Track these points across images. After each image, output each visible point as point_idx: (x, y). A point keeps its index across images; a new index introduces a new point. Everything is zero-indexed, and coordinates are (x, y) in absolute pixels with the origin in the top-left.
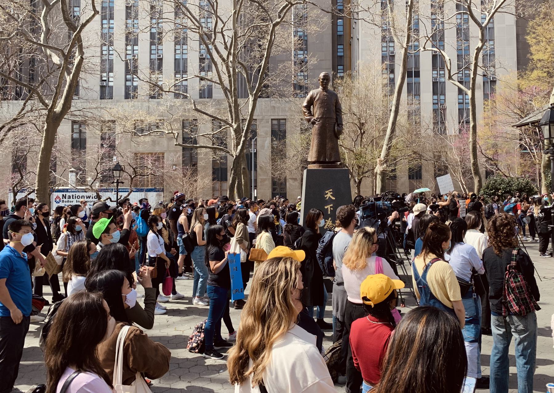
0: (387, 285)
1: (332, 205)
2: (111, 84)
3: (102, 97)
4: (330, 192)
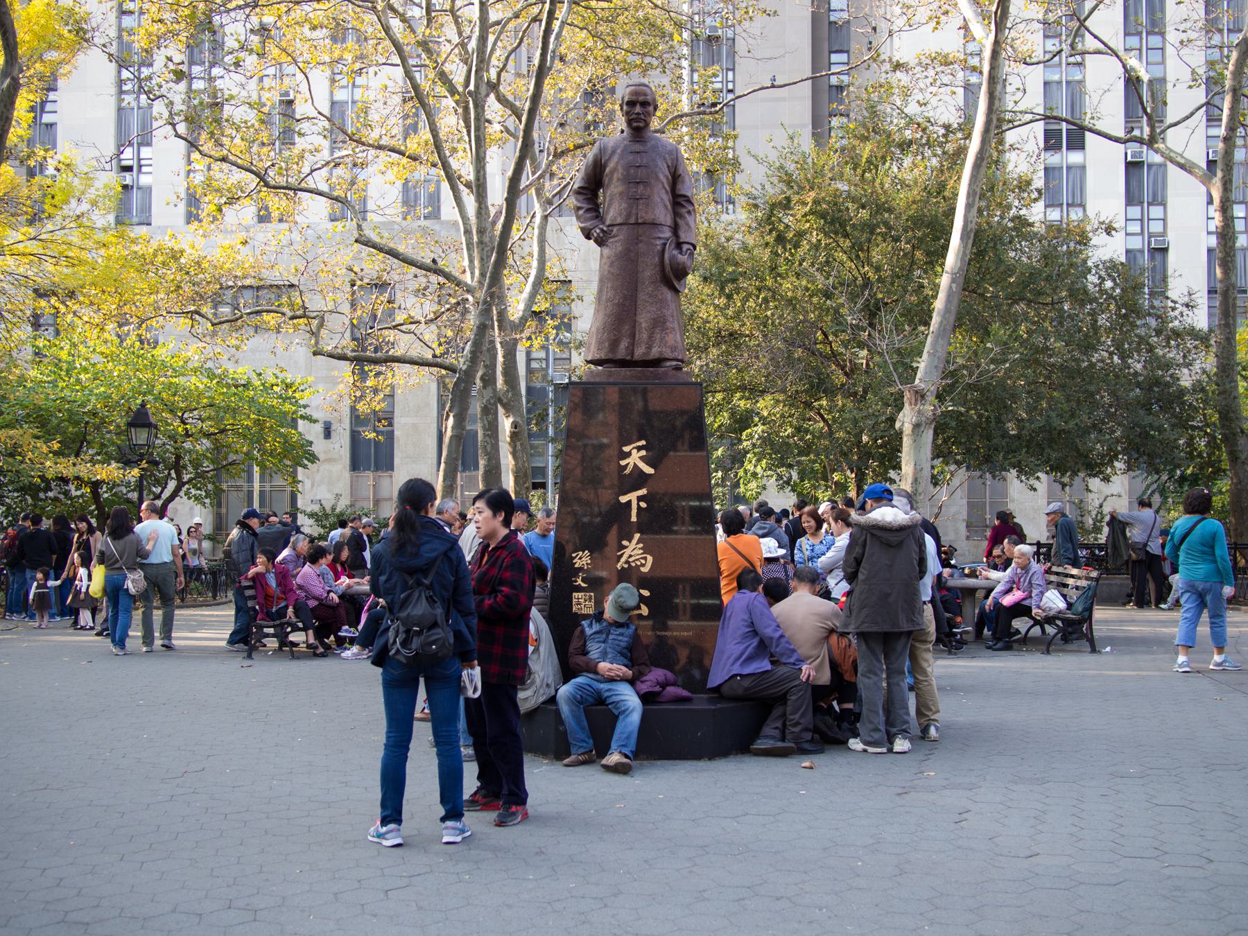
0: (486, 807)
1: (643, 492)
2: (144, 180)
3: (150, 224)
4: (639, 449)
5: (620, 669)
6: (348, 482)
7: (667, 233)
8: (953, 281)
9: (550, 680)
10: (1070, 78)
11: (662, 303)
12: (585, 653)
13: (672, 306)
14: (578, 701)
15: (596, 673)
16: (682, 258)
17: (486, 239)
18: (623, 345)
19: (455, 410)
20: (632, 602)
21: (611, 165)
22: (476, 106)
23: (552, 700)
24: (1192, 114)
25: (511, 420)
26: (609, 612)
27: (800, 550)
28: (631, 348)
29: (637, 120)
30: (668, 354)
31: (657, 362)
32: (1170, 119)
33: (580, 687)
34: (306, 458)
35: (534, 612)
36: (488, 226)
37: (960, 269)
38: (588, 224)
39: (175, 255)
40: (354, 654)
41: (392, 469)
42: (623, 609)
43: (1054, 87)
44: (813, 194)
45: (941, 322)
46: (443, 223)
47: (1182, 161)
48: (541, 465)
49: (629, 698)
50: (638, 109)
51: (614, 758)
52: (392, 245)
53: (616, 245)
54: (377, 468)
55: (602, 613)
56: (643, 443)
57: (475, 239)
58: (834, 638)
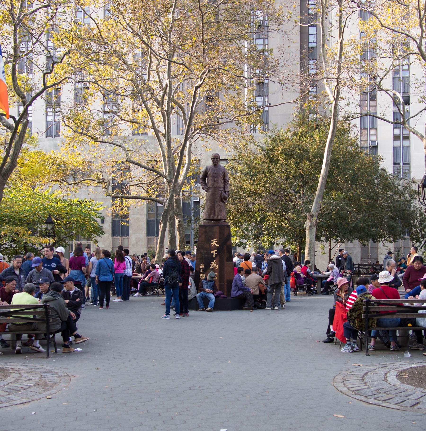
1: (216, 250)
4: (215, 240)
5: (211, 290)
6: (111, 241)
7: (222, 189)
8: (323, 179)
9: (195, 293)
10: (403, 76)
11: (221, 206)
12: (203, 287)
13: (224, 207)
14: (201, 297)
15: (205, 291)
16: (226, 195)
17: (171, 160)
18: (212, 216)
19: (163, 222)
20: (213, 276)
21: (209, 173)
22: (167, 115)
23: (195, 297)
24: (419, 113)
25: (178, 220)
26: (208, 278)
27: (263, 265)
28: (214, 217)
29: (215, 162)
30: (223, 218)
31: (220, 220)
32: (412, 115)
33: (201, 294)
34: (100, 233)
35: (190, 278)
36: (171, 155)
37: (325, 176)
38: (203, 187)
39: (55, 159)
40: (137, 295)
41: (129, 236)
42: (212, 277)
43: (397, 79)
44: (281, 147)
45: (319, 193)
46: (149, 137)
47: (414, 131)
48: (188, 234)
49: (213, 297)
50: (215, 160)
51: (209, 309)
52: (139, 162)
53: (210, 192)
54: (123, 235)
55: (207, 278)
56: (216, 239)
57: (167, 159)
58: (260, 284)
